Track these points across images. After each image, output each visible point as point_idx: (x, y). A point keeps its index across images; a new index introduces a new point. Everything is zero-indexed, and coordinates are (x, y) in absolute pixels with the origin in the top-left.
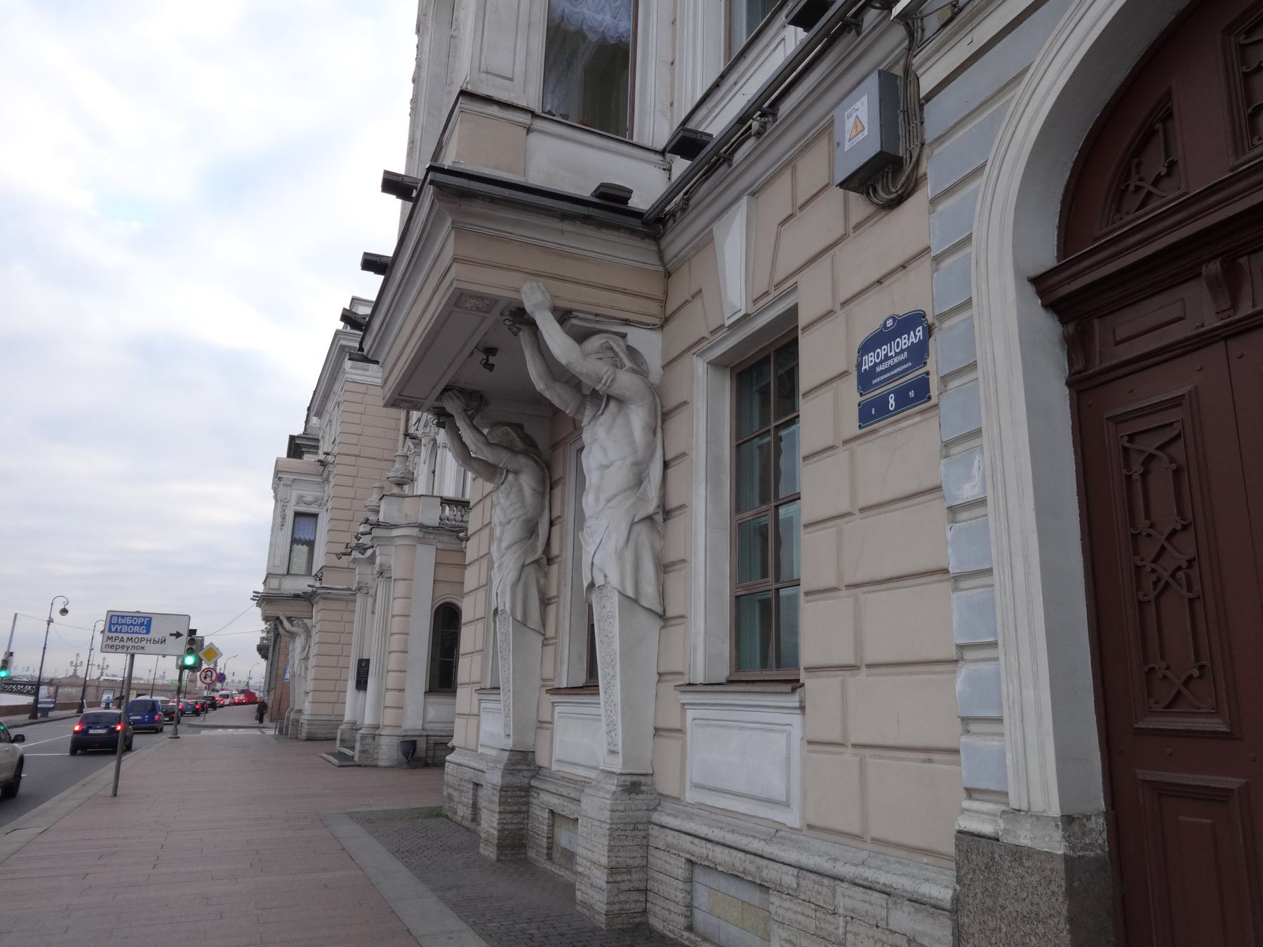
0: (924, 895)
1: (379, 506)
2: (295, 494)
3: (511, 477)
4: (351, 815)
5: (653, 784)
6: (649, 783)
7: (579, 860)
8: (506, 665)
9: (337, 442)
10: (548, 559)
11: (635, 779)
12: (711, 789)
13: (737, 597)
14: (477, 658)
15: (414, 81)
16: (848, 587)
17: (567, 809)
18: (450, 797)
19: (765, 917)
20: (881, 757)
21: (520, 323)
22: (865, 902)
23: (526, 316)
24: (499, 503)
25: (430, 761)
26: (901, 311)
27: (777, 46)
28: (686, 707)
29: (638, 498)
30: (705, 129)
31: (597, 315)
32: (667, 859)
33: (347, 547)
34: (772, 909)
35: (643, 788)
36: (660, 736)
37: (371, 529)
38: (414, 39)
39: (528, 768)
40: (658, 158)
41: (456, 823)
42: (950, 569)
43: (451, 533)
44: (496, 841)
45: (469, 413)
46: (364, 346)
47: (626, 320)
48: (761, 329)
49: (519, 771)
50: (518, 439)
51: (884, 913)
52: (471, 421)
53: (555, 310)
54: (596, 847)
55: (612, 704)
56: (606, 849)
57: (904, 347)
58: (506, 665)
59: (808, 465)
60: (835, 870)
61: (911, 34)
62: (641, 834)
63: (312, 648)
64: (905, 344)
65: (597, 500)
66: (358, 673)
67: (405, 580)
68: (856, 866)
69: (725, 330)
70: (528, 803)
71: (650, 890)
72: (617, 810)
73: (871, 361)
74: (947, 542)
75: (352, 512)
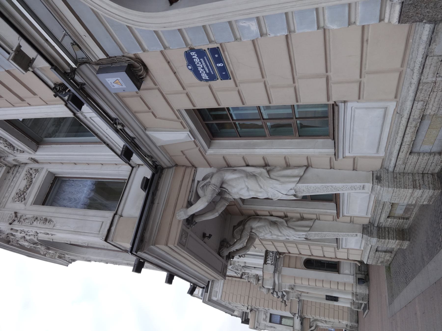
0: (428, 38)
1: (267, 288)
2: (263, 322)
3: (253, 231)
4: (390, 304)
5: (377, 171)
6: (376, 173)
7: (410, 203)
8: (327, 235)
9: (243, 304)
10: (285, 217)
11: (375, 178)
12: (379, 145)
13: (299, 136)
14: (325, 249)
15: (107, 263)
16: (294, 82)
17: (387, 209)
18: (382, 262)
19: (436, 117)
20: (366, 64)
21: (192, 221)
22: (430, 68)
23: (190, 219)
24: (264, 236)
25: (366, 273)
26: (185, 62)
27: (93, 121)
28: (344, 156)
29: (260, 176)
30: (121, 147)
31: (190, 192)
32: (409, 164)
33: (282, 302)
34: (432, 113)
35: (379, 175)
36: (356, 168)
37: (276, 292)
38: (93, 262)
39: (370, 227)
40: (134, 169)
41: (392, 260)
42: (286, 34)
43: (277, 261)
44: (401, 241)
45: (228, 246)
46: (202, 287)
47: (192, 181)
48: (195, 126)
49: (371, 231)
50: (239, 228)
51: (435, 58)
52: (231, 245)
53: (187, 207)
54: (404, 194)
55: (343, 187)
56: (405, 190)
57: (199, 60)
58: (327, 235)
59: (246, 103)
60: (416, 83)
61: (84, 63)
62: (398, 176)
63: (322, 319)
64: (197, 60)
65: (261, 192)
66: (332, 300)
67: (295, 280)
68: (413, 73)
69: (196, 141)
70: (385, 228)
71: (423, 172)
72: (388, 185)
73: (205, 75)
74: (275, 36)
75: (270, 300)
